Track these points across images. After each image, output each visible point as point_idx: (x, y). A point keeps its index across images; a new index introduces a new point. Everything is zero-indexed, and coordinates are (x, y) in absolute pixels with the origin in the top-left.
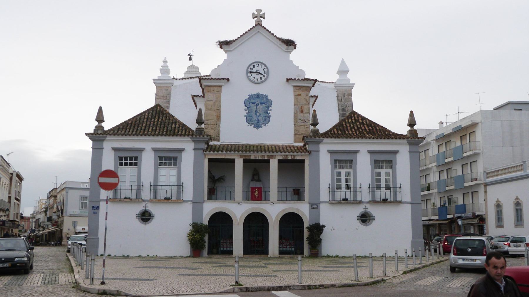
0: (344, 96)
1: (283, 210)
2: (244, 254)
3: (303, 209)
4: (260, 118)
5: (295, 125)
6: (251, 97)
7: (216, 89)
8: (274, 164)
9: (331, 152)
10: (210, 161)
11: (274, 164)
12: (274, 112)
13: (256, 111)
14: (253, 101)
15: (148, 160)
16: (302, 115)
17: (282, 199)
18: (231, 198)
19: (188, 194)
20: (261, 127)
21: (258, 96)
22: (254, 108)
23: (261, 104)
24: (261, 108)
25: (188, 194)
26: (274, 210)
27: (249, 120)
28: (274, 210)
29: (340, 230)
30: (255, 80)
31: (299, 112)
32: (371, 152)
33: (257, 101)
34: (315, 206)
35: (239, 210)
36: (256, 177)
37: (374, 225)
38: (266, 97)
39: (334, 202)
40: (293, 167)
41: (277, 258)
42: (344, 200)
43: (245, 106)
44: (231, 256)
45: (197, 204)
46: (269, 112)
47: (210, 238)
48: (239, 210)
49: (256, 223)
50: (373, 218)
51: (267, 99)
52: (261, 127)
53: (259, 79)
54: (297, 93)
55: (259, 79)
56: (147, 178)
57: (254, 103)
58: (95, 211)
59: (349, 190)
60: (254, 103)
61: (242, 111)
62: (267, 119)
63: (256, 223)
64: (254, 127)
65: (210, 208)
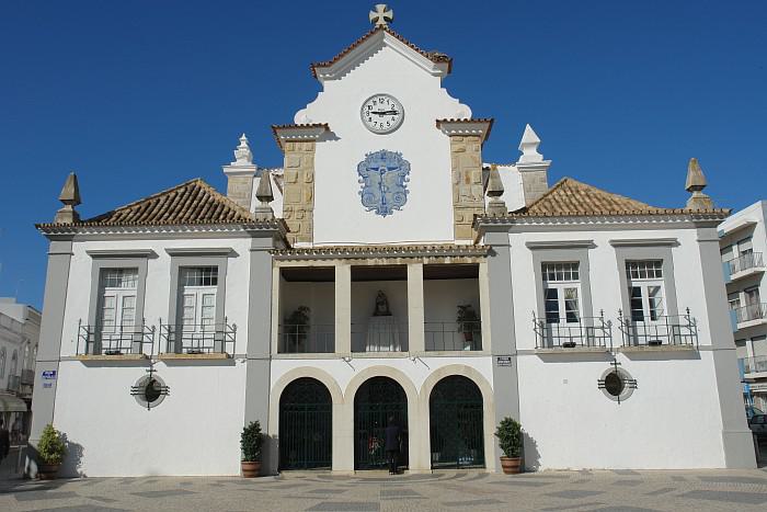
0: (534, 182)
1: (439, 371)
2: (357, 467)
3: (478, 366)
4: (388, 196)
5: (456, 207)
6: (370, 157)
7: (305, 145)
8: (415, 274)
9: (533, 247)
10: (283, 271)
11: (415, 274)
12: (413, 183)
13: (380, 184)
14: (374, 165)
15: (160, 276)
16: (468, 187)
17: (433, 344)
18: (327, 346)
19: (240, 345)
20: (391, 213)
21: (383, 155)
22: (376, 176)
23: (390, 169)
24: (389, 177)
25: (240, 345)
26: (417, 372)
27: (367, 199)
28: (417, 372)
29: (556, 408)
30: (378, 126)
31: (463, 181)
32: (617, 245)
33: (382, 165)
34: (505, 360)
35: (342, 373)
36: (382, 308)
37: (633, 401)
38: (398, 156)
39: (546, 350)
40: (454, 278)
41: (427, 476)
42: (653, 344)
43: (360, 174)
44: (327, 473)
45: (258, 363)
46: (404, 184)
47: (294, 436)
48: (342, 373)
49: (380, 399)
50: (634, 384)
51: (400, 160)
52: (391, 213)
53: (385, 125)
54: (458, 147)
55: (385, 125)
56: (158, 308)
57: (377, 169)
58: (48, 382)
59: (577, 324)
60: (377, 169)
61: (355, 185)
62: (401, 197)
63: (380, 399)
64: (377, 213)
65: (288, 368)
